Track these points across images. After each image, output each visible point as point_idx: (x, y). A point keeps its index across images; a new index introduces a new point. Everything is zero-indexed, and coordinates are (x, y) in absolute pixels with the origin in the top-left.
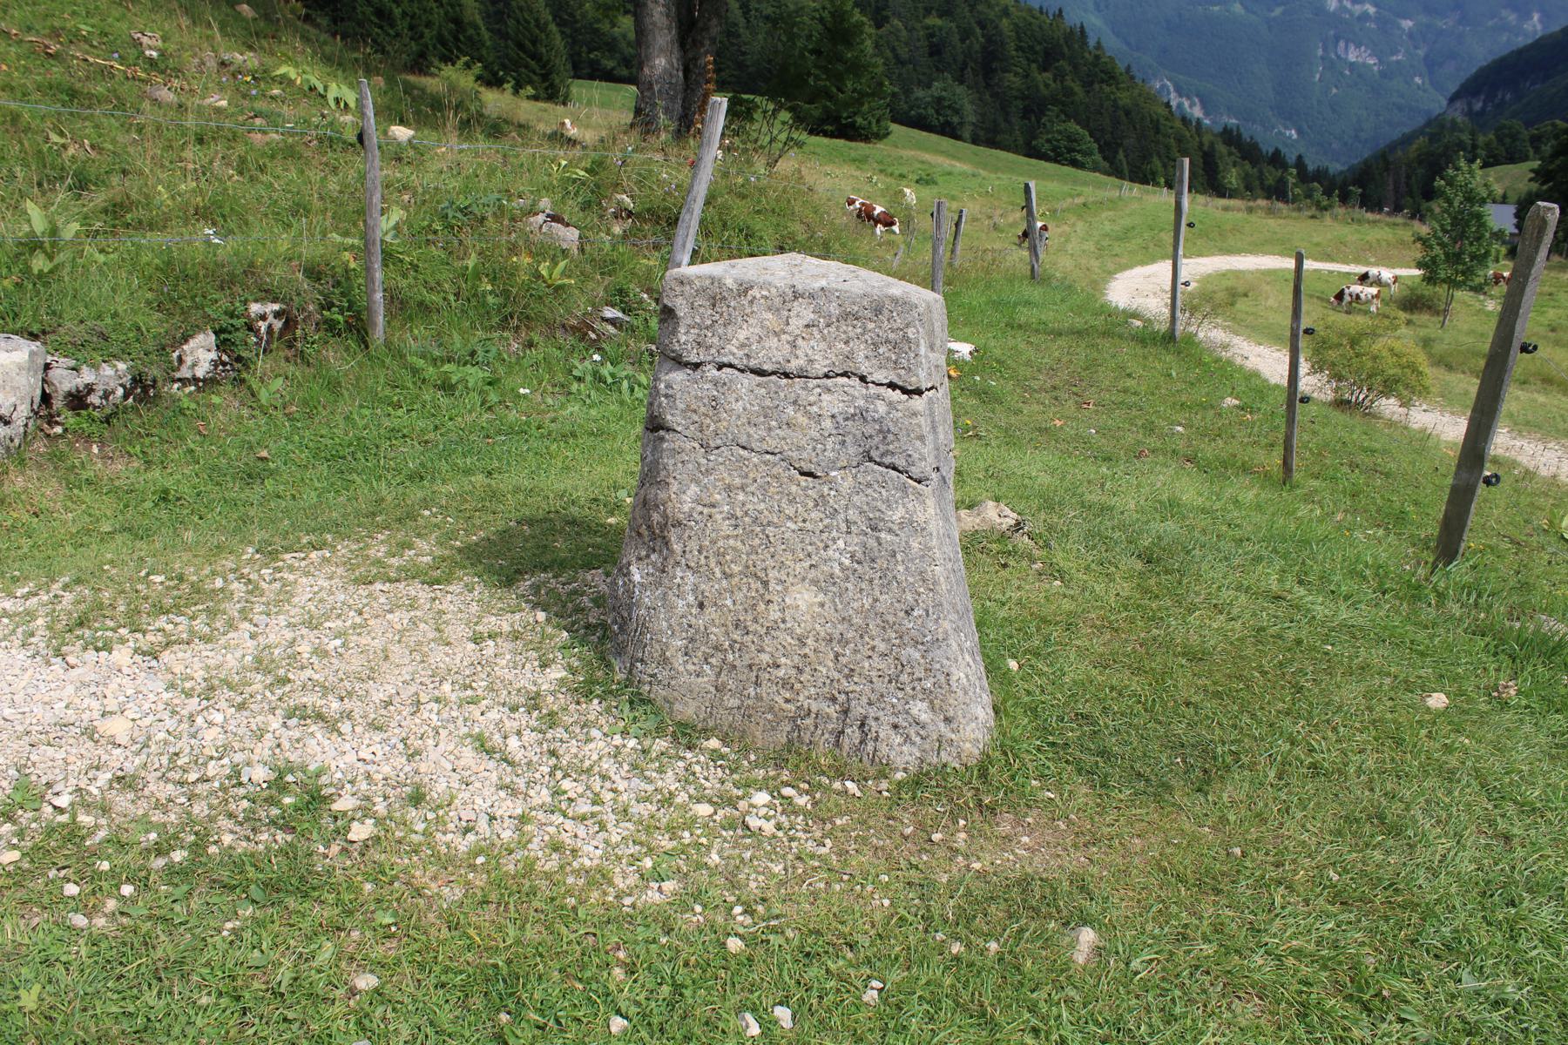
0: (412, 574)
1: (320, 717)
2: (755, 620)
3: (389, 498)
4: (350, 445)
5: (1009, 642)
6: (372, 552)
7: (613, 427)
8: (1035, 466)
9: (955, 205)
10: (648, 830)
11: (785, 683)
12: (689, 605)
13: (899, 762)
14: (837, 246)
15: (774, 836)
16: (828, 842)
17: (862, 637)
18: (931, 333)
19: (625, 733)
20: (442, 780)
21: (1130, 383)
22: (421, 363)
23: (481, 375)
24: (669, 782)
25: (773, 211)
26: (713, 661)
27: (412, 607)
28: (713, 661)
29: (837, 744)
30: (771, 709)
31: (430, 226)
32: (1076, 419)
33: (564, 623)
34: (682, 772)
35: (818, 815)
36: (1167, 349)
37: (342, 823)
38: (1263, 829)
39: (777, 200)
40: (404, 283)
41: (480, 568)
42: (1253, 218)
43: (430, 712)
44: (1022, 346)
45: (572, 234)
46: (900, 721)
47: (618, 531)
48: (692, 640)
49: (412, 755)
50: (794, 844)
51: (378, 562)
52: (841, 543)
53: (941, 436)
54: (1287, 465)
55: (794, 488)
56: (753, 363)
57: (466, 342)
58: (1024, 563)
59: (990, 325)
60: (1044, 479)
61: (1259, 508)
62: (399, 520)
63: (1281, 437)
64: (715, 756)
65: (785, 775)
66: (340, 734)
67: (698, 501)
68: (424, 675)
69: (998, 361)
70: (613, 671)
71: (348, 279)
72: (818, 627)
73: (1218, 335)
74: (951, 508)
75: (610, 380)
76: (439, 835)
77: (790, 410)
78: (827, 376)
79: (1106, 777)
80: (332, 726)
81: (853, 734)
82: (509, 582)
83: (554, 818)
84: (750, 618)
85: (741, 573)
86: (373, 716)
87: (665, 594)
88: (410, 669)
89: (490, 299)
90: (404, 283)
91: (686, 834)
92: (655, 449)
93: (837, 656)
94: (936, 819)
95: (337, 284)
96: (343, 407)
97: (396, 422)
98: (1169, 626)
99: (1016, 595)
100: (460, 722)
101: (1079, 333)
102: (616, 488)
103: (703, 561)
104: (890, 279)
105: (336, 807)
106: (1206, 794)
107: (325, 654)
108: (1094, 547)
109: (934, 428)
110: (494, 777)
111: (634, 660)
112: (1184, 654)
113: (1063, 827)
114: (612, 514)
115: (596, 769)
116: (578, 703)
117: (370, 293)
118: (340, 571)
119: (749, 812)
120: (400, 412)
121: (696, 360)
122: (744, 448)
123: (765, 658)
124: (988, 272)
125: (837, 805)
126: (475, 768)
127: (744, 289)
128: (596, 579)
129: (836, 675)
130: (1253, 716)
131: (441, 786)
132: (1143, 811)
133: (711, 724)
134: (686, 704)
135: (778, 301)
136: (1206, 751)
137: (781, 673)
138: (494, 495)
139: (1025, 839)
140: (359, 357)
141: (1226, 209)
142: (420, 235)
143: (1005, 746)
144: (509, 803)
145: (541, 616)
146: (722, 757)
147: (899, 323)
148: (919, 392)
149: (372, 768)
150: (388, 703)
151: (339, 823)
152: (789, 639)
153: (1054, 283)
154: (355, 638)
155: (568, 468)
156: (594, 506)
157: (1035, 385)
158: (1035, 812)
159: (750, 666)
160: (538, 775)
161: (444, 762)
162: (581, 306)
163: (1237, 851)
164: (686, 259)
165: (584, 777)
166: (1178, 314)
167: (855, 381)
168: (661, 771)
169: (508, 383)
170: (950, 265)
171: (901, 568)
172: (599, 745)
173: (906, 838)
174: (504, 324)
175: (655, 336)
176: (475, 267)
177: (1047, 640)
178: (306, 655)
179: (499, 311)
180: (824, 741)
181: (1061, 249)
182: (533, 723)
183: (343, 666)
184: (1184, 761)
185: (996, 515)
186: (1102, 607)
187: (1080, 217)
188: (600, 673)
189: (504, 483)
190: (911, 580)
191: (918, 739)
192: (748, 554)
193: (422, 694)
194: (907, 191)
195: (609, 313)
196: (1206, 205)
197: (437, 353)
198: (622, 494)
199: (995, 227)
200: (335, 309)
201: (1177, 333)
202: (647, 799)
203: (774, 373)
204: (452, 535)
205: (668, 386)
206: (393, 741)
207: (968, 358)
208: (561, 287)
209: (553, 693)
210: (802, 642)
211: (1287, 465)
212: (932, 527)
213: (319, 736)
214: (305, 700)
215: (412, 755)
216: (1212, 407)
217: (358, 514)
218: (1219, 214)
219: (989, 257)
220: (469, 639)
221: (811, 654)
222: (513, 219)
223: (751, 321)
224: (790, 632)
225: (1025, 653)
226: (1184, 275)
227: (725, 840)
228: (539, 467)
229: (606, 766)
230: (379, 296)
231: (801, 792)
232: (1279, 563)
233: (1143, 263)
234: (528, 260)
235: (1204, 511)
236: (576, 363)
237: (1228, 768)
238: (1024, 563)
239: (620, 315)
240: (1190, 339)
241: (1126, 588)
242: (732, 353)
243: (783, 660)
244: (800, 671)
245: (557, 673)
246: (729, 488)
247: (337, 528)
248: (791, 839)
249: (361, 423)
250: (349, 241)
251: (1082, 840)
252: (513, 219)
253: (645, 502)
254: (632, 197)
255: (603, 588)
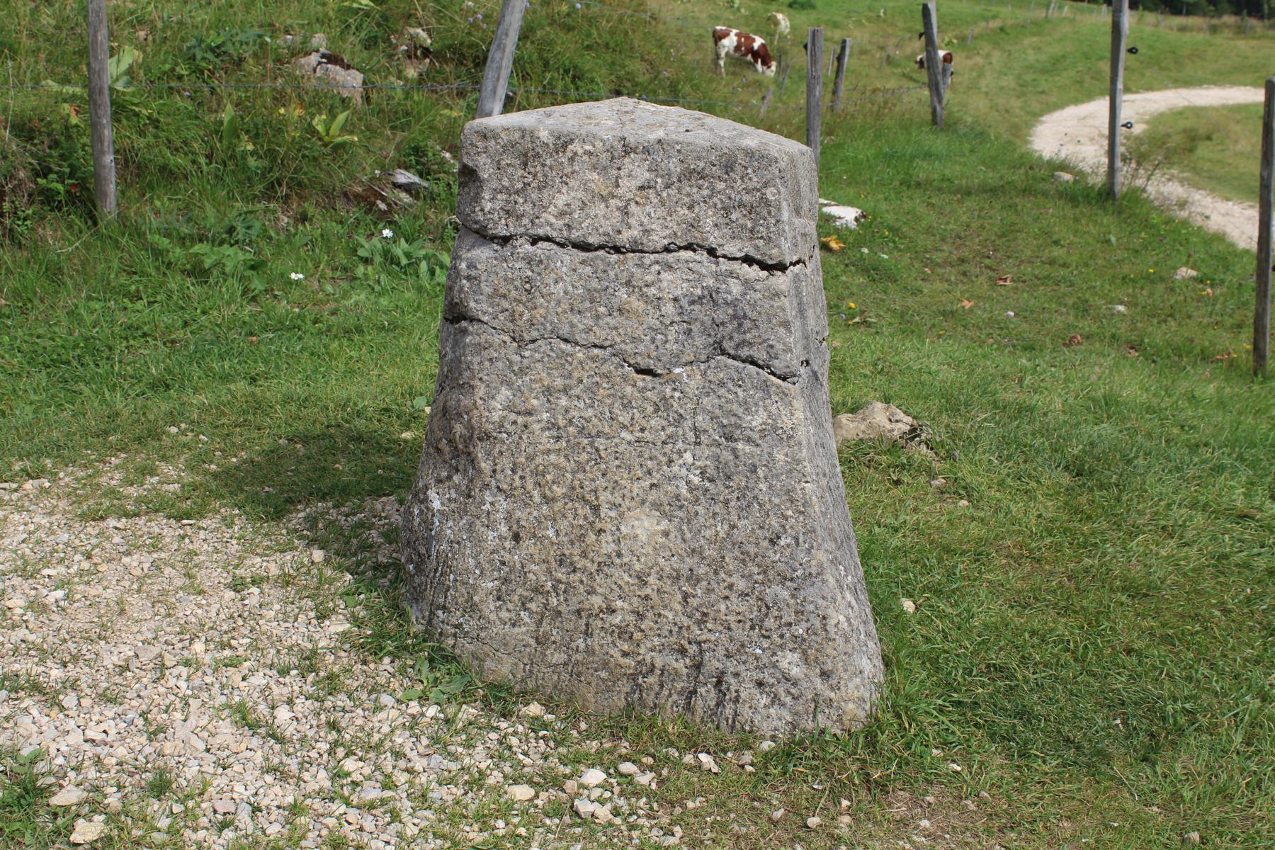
0: (156, 506)
1: (35, 687)
2: (584, 555)
3: (126, 413)
4: (76, 346)
5: (902, 577)
6: (103, 480)
7: (409, 319)
8: (936, 359)
9: (838, 35)
10: (454, 819)
11: (622, 632)
12: (501, 538)
13: (766, 728)
14: (687, 89)
15: (610, 824)
16: (677, 830)
17: (716, 572)
18: (796, 193)
19: (423, 699)
20: (193, 762)
21: (1058, 252)
22: (165, 243)
23: (241, 256)
24: (479, 758)
25: (607, 46)
26: (533, 606)
27: (155, 548)
28: (533, 606)
29: (689, 707)
30: (605, 665)
31: (173, 70)
32: (991, 298)
33: (348, 563)
34: (494, 746)
35: (666, 797)
36: (1105, 209)
37: (65, 818)
38: (1228, 807)
39: (612, 32)
40: (141, 142)
41: (242, 497)
42: (1218, 39)
43: (178, 679)
44: (921, 209)
45: (351, 80)
46: (766, 676)
47: (414, 448)
48: (506, 581)
49: (155, 733)
50: (635, 834)
51: (112, 493)
52: (688, 457)
53: (811, 322)
54: (1258, 351)
55: (629, 390)
56: (575, 235)
57: (222, 215)
58: (922, 479)
59: (881, 183)
60: (947, 374)
61: (1221, 404)
62: (139, 440)
63: (1251, 314)
64: (537, 724)
65: (624, 748)
66: (62, 709)
67: (510, 408)
68: (170, 632)
69: (891, 229)
70: (408, 621)
71: (69, 138)
72: (662, 561)
73: (1174, 190)
74: (826, 414)
75: (404, 261)
76: (188, 833)
77: (622, 293)
78: (667, 250)
79: (1025, 744)
80: (51, 699)
81: (707, 694)
82: (278, 514)
83: (334, 807)
84: (576, 551)
85: (565, 495)
86: (104, 685)
87: (471, 524)
88: (152, 624)
89: (252, 162)
90: (141, 142)
91: (501, 824)
92: (456, 344)
93: (686, 597)
94: (814, 797)
95: (55, 144)
96: (67, 299)
97: (134, 319)
98: (1104, 554)
99: (911, 519)
100: (216, 689)
101: (993, 191)
102: (412, 394)
103: (518, 483)
104: (745, 128)
105: (56, 801)
106: (1154, 764)
107: (44, 608)
108: (1009, 458)
109: (801, 312)
110: (258, 757)
111: (434, 607)
112: (1124, 590)
113: (972, 807)
114: (407, 427)
115: (388, 744)
116: (365, 662)
117: (97, 156)
118: (63, 504)
119: (578, 795)
120: (139, 305)
121: (504, 233)
122: (566, 341)
123: (597, 601)
124: (878, 116)
125: (688, 784)
126: (234, 747)
127: (563, 143)
128: (387, 506)
129: (686, 621)
130: (1213, 666)
131: (191, 771)
132: (1074, 787)
133: (531, 684)
134: (500, 661)
135: (604, 158)
136: (1153, 710)
137: (617, 619)
138: (258, 406)
139: (925, 823)
140: (85, 237)
141: (1183, 29)
142: (158, 81)
143: (898, 703)
144: (277, 790)
145: (318, 555)
146: (545, 726)
147: (755, 182)
148: (782, 267)
149: (102, 751)
150: (124, 669)
151: (60, 821)
152: (627, 578)
153: (962, 130)
154: (81, 588)
155: (353, 372)
156: (384, 418)
157: (938, 257)
158: (936, 789)
159: (579, 612)
160: (314, 754)
161: (196, 740)
162: (368, 170)
163: (1195, 836)
164: (498, 106)
165: (372, 755)
166: (1119, 164)
167: (703, 256)
168: (469, 745)
169: (276, 266)
170: (832, 109)
171: (763, 486)
172: (390, 715)
173: (775, 823)
174: (270, 193)
175: (452, 200)
176: (232, 121)
177: (950, 574)
178: (18, 611)
179: (263, 176)
180: (672, 703)
181: (973, 87)
182: (308, 689)
183: (66, 623)
184: (1125, 723)
185: (886, 419)
186: (1020, 532)
187: (996, 45)
188: (392, 625)
189: (272, 390)
190: (776, 501)
191: (788, 700)
192: (573, 473)
193: (167, 656)
194: (780, 16)
195: (403, 177)
196: (1156, 26)
197: (185, 230)
198: (420, 402)
199: (889, 61)
200: (52, 176)
201: (1117, 188)
202: (452, 781)
203: (601, 247)
204: (205, 457)
205: (471, 266)
206: (130, 716)
207: (853, 225)
208: (342, 145)
209: (332, 651)
210: (642, 580)
211: (1258, 351)
212: (801, 434)
213: (35, 712)
214: (17, 667)
215: (155, 733)
216: (1162, 279)
217: (86, 433)
218: (1174, 36)
219: (880, 98)
220: (228, 586)
221: (654, 595)
222: (279, 60)
223: (572, 183)
224: (627, 567)
225: (923, 590)
226: (1124, 114)
227: (549, 830)
228: (316, 371)
229: (399, 741)
230: (109, 158)
231: (644, 769)
232: (1245, 474)
233: (1076, 101)
234: (298, 112)
235: (1150, 410)
236: (362, 241)
237: (1181, 731)
238: (922, 479)
239: (416, 179)
240: (1135, 196)
241: (1050, 508)
242: (550, 223)
243: (619, 603)
244: (641, 617)
245: (337, 626)
246: (548, 391)
247: (59, 451)
248: (632, 827)
249: (89, 319)
250: (69, 90)
251: (996, 823)
252: (279, 60)
253: (445, 411)
254: (428, 31)
255: (397, 519)
